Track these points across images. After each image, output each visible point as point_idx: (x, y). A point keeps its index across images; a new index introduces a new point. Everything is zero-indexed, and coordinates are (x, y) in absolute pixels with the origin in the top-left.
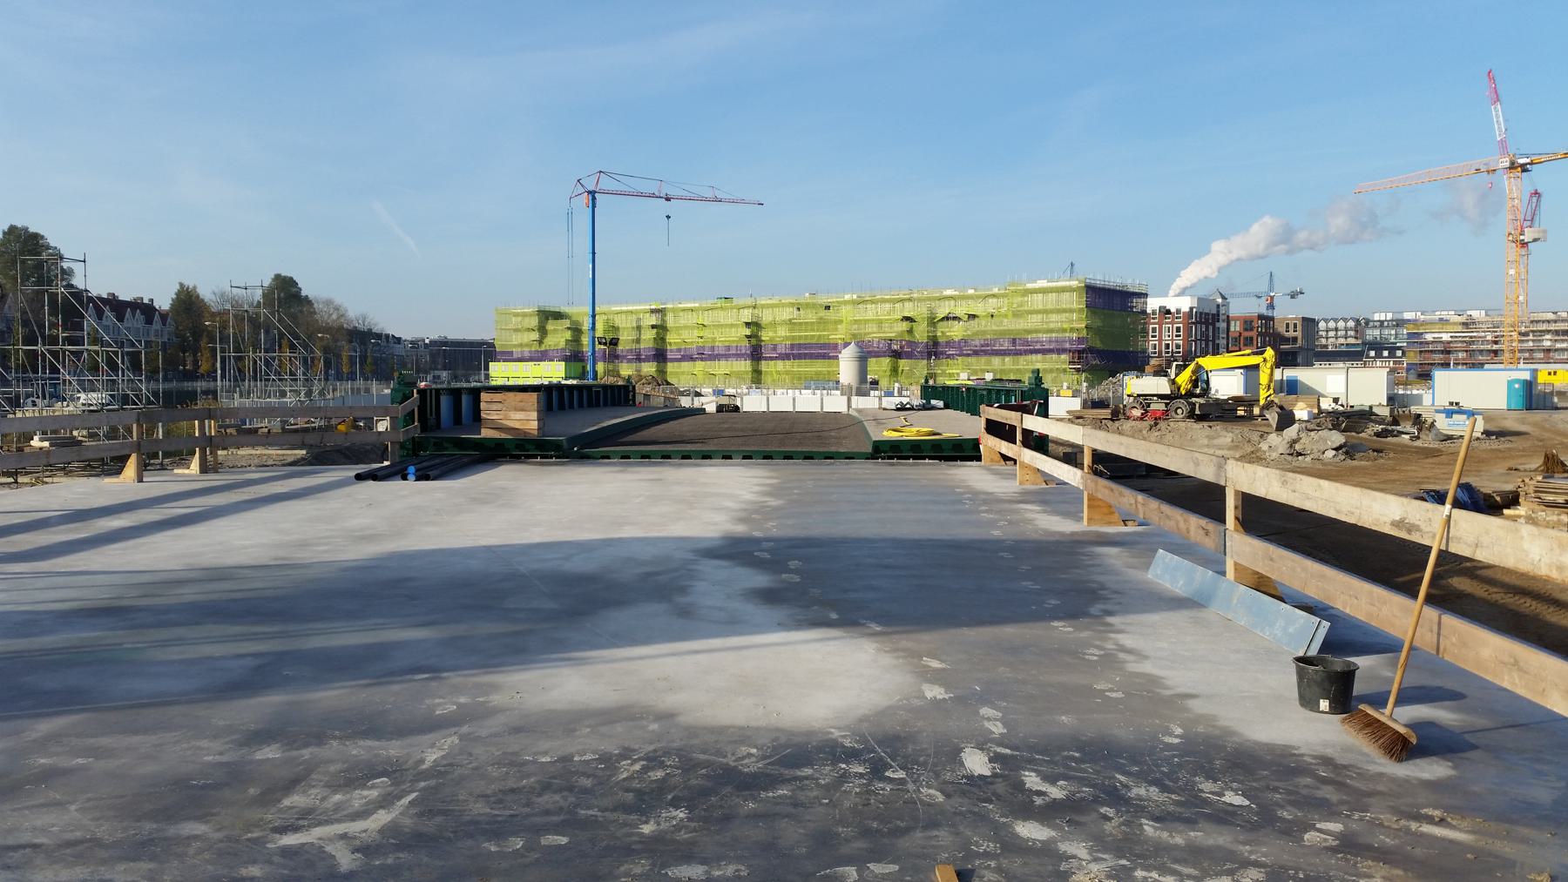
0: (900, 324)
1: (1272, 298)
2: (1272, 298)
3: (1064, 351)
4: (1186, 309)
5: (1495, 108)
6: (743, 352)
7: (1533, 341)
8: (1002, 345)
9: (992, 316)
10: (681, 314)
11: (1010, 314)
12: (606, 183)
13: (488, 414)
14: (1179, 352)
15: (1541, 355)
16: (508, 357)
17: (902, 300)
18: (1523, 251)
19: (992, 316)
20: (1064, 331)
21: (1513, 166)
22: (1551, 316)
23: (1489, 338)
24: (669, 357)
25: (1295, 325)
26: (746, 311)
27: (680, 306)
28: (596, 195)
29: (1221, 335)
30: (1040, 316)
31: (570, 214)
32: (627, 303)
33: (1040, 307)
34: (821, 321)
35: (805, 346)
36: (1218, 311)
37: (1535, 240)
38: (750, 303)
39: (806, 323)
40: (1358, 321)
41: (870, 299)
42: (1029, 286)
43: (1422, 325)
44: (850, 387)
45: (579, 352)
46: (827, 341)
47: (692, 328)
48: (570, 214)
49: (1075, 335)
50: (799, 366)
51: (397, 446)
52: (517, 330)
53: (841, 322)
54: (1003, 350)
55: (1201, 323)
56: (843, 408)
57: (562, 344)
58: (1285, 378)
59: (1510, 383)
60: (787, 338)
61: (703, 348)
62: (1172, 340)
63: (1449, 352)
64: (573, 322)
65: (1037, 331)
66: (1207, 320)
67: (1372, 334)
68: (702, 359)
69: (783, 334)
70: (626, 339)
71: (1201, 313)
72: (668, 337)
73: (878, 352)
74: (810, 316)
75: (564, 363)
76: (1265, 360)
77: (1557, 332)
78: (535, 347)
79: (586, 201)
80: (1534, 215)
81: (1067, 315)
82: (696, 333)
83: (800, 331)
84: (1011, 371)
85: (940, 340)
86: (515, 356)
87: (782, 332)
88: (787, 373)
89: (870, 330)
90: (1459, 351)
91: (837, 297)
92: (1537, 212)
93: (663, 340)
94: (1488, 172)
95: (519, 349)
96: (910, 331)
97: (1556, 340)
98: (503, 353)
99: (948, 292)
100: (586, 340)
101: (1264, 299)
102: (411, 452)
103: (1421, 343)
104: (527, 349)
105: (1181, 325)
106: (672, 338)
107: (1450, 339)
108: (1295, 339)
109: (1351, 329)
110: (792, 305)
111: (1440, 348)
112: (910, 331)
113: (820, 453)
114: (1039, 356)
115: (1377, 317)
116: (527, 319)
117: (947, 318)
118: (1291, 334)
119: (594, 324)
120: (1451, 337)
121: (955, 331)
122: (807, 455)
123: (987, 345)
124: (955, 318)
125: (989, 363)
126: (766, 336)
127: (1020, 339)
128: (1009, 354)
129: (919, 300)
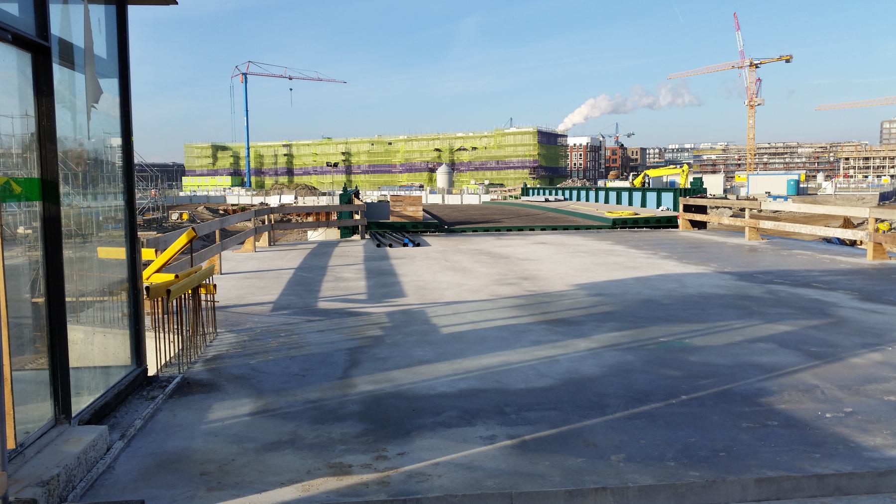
0: (435, 152)
1: (617, 137)
2: (617, 137)
3: (526, 167)
4: (584, 144)
5: (738, 33)
6: (341, 169)
7: (758, 158)
8: (491, 165)
9: (486, 148)
10: (302, 147)
11: (496, 147)
12: (253, 69)
13: (395, 208)
14: (581, 168)
15: (762, 166)
16: (193, 174)
17: (433, 139)
18: (752, 111)
19: (486, 148)
20: (526, 156)
21: (751, 65)
22: (767, 146)
23: (736, 157)
24: (295, 173)
25: (637, 152)
26: (341, 145)
27: (300, 142)
28: (248, 76)
29: (602, 158)
30: (512, 148)
31: (232, 87)
32: (268, 141)
33: (512, 143)
34: (387, 151)
35: (381, 166)
36: (601, 145)
37: (759, 105)
38: (342, 141)
39: (378, 153)
40: (660, 150)
41: (414, 138)
42: (506, 131)
43: (701, 151)
44: (443, 189)
45: (238, 170)
46: (390, 163)
47: (309, 155)
48: (232, 87)
49: (532, 159)
50: (374, 178)
51: (364, 228)
52: (198, 157)
53: (398, 152)
54: (492, 167)
55: (592, 151)
56: (440, 202)
57: (228, 166)
58: (668, 181)
59: (789, 181)
60: (367, 161)
61: (316, 167)
62: (578, 161)
63: (715, 165)
64: (234, 152)
65: (511, 157)
66: (595, 149)
67: (668, 156)
68: (316, 174)
69: (365, 159)
70: (268, 162)
71: (592, 146)
72: (294, 161)
73: (421, 169)
74: (377, 148)
75: (230, 177)
76: (683, 171)
77: (770, 154)
78: (211, 167)
79: (241, 79)
80: (758, 91)
81: (528, 147)
82: (312, 159)
83: (374, 157)
84: (497, 179)
85: (456, 162)
86: (198, 173)
87: (364, 158)
88: (367, 181)
89: (416, 156)
90: (720, 164)
91: (395, 138)
92: (760, 90)
93: (291, 163)
94: (739, 68)
95: (200, 169)
96: (439, 157)
97: (770, 158)
98: (189, 171)
99: (460, 135)
100: (243, 163)
101: (613, 138)
102: (351, 231)
103: (701, 160)
104: (205, 169)
105: (582, 153)
106: (297, 163)
107: (716, 158)
108: (637, 160)
109: (657, 154)
110: (369, 142)
111: (711, 163)
112: (439, 157)
113: (572, 226)
114: (512, 171)
115: (670, 147)
116: (204, 151)
117: (459, 149)
118: (635, 157)
119: (249, 153)
120: (717, 157)
121: (465, 157)
122: (520, 228)
123: (483, 165)
124: (464, 149)
125: (484, 175)
126: (354, 160)
127: (501, 161)
128: (496, 170)
129: (443, 139)
